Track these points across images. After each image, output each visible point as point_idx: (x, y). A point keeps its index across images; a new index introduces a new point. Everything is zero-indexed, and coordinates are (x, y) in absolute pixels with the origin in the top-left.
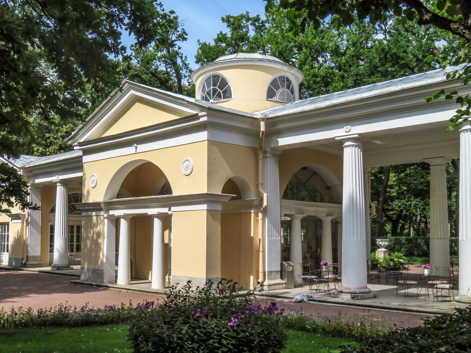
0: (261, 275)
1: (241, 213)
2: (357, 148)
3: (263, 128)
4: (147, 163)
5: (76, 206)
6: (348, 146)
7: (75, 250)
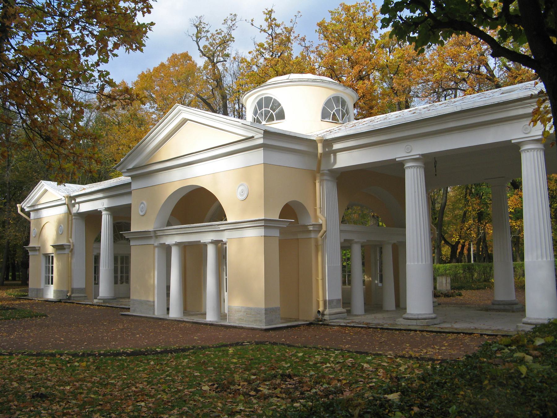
0: (321, 304)
1: (298, 239)
2: (418, 169)
3: (320, 150)
4: (196, 189)
5: (124, 235)
6: (409, 167)
7: (119, 282)
